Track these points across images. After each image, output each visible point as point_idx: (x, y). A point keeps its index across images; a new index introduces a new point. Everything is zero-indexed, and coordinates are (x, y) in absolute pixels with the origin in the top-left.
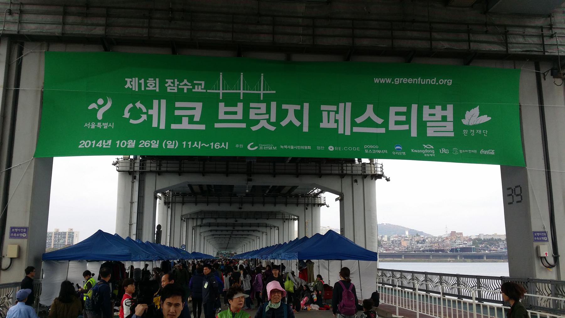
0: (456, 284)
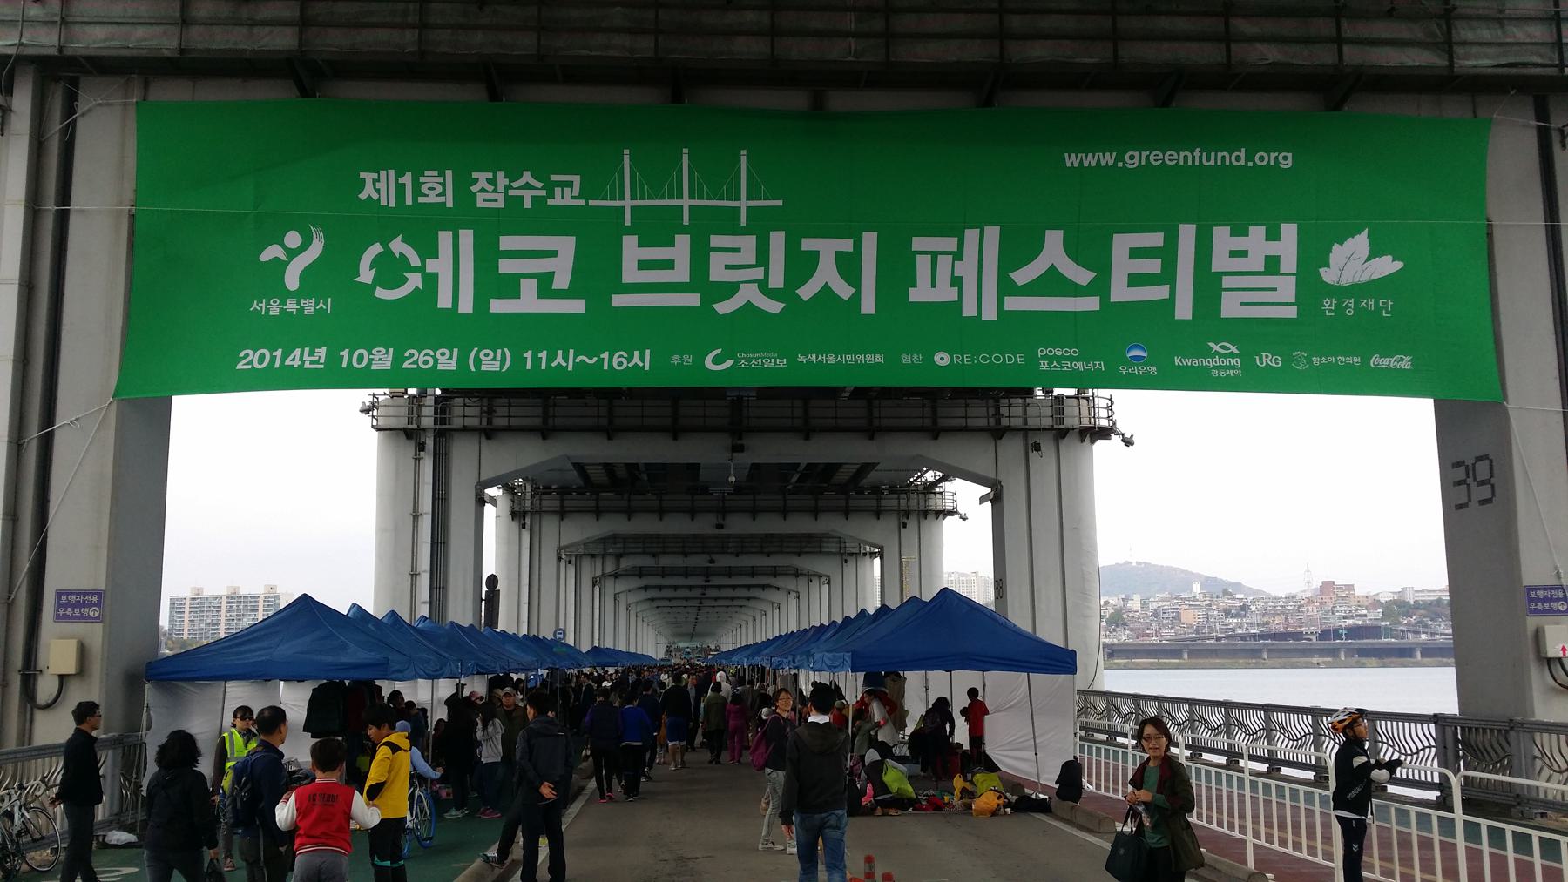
0: (1310, 734)
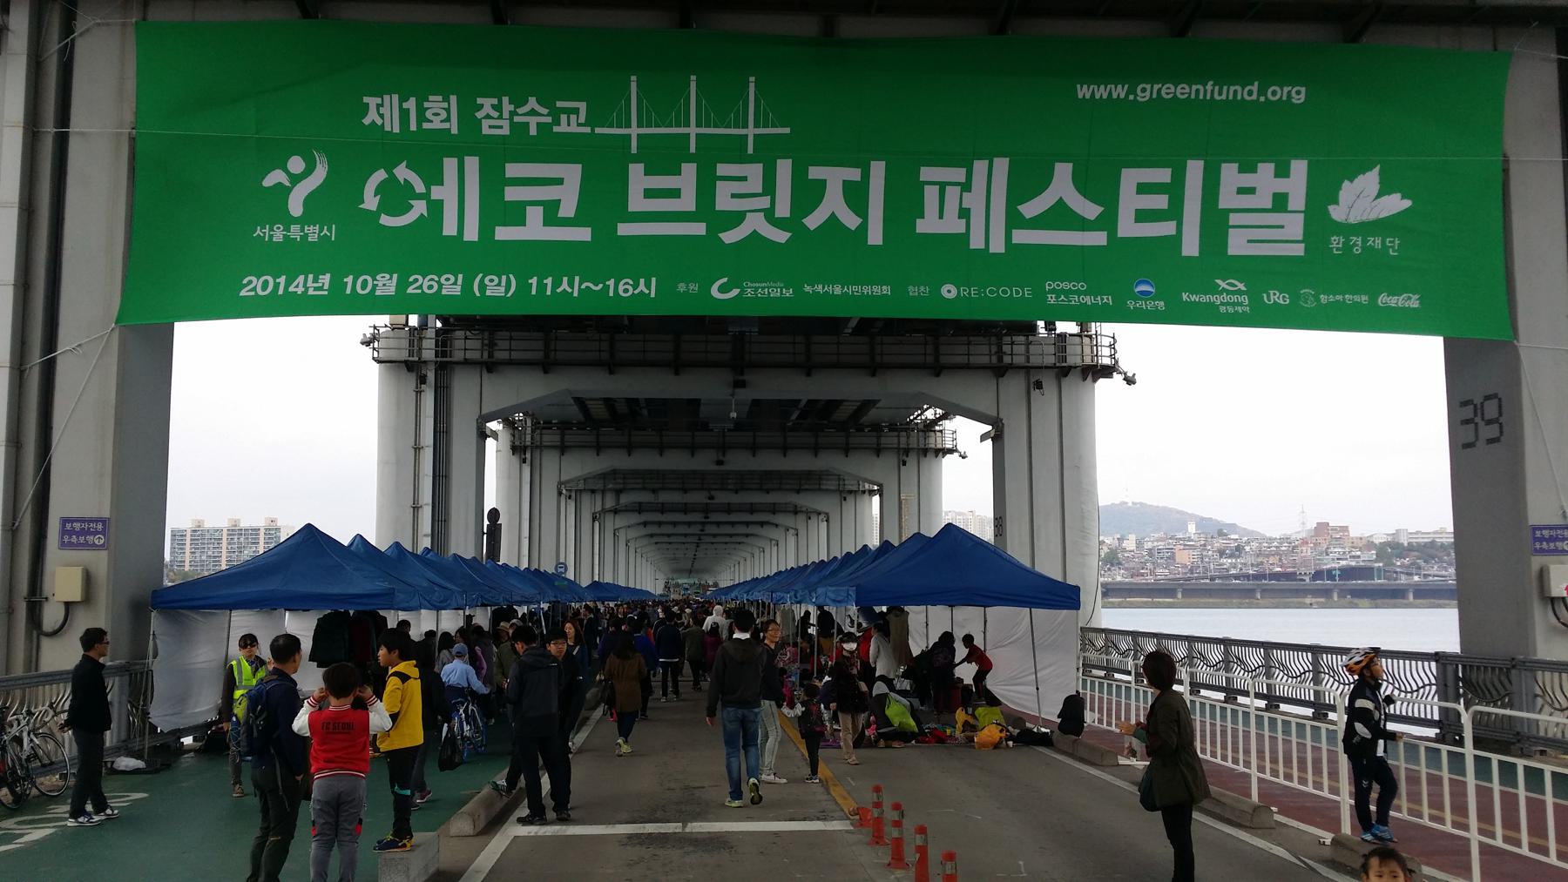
0: (1309, 671)
